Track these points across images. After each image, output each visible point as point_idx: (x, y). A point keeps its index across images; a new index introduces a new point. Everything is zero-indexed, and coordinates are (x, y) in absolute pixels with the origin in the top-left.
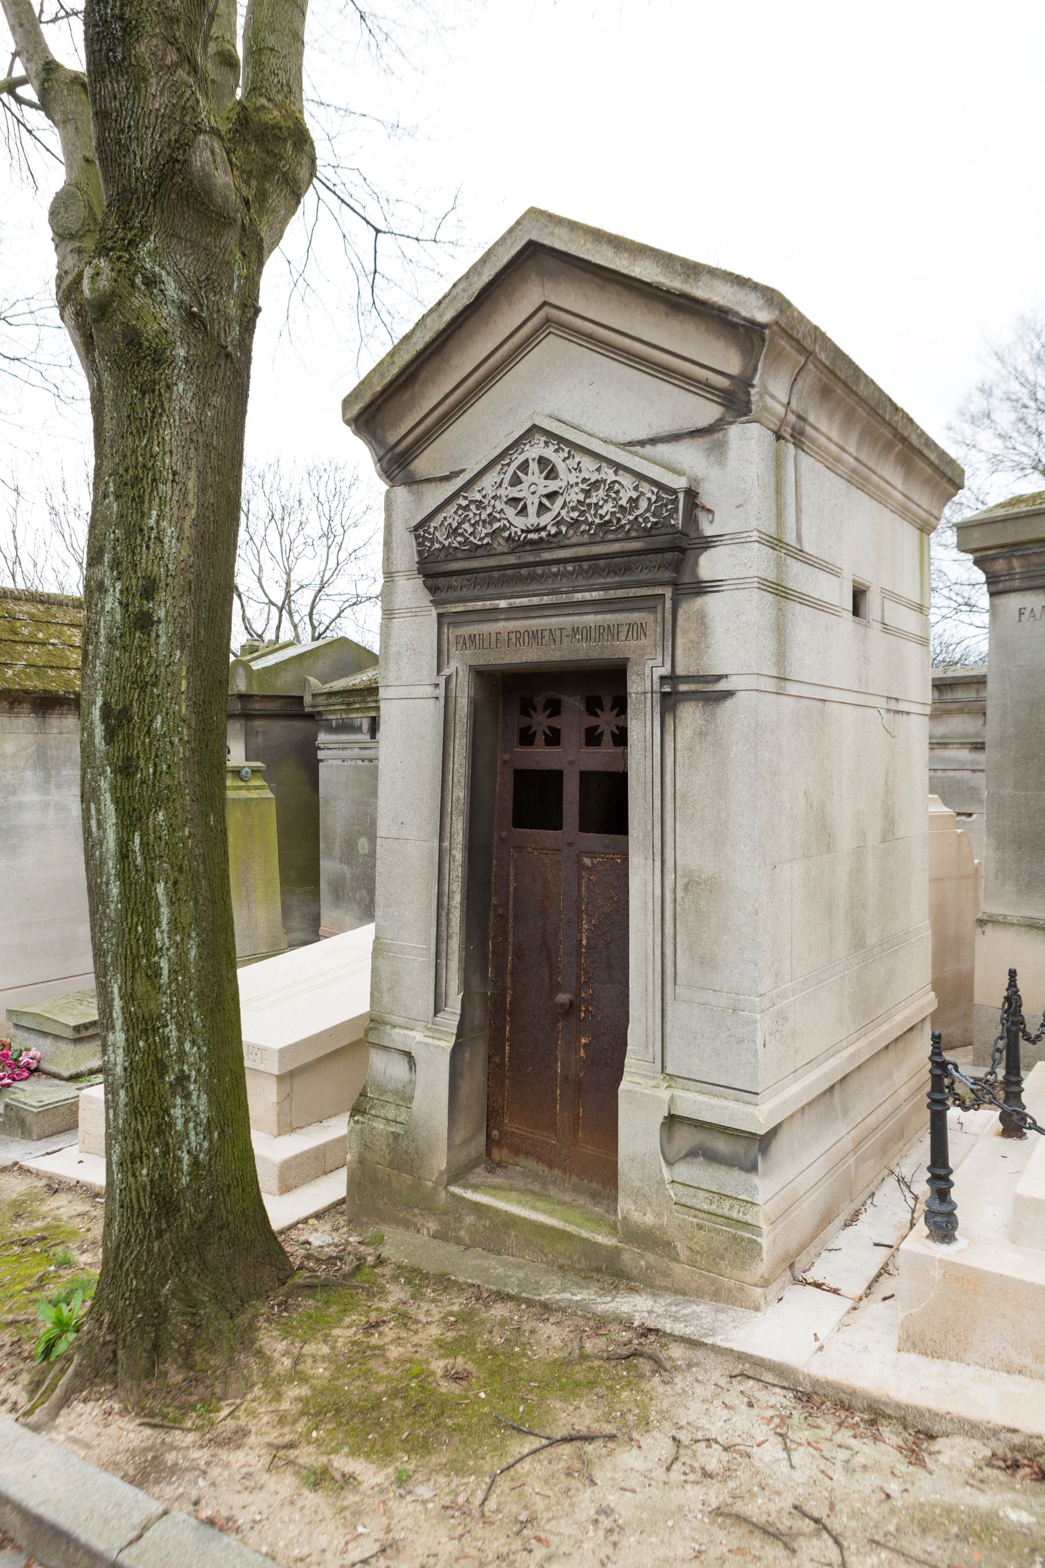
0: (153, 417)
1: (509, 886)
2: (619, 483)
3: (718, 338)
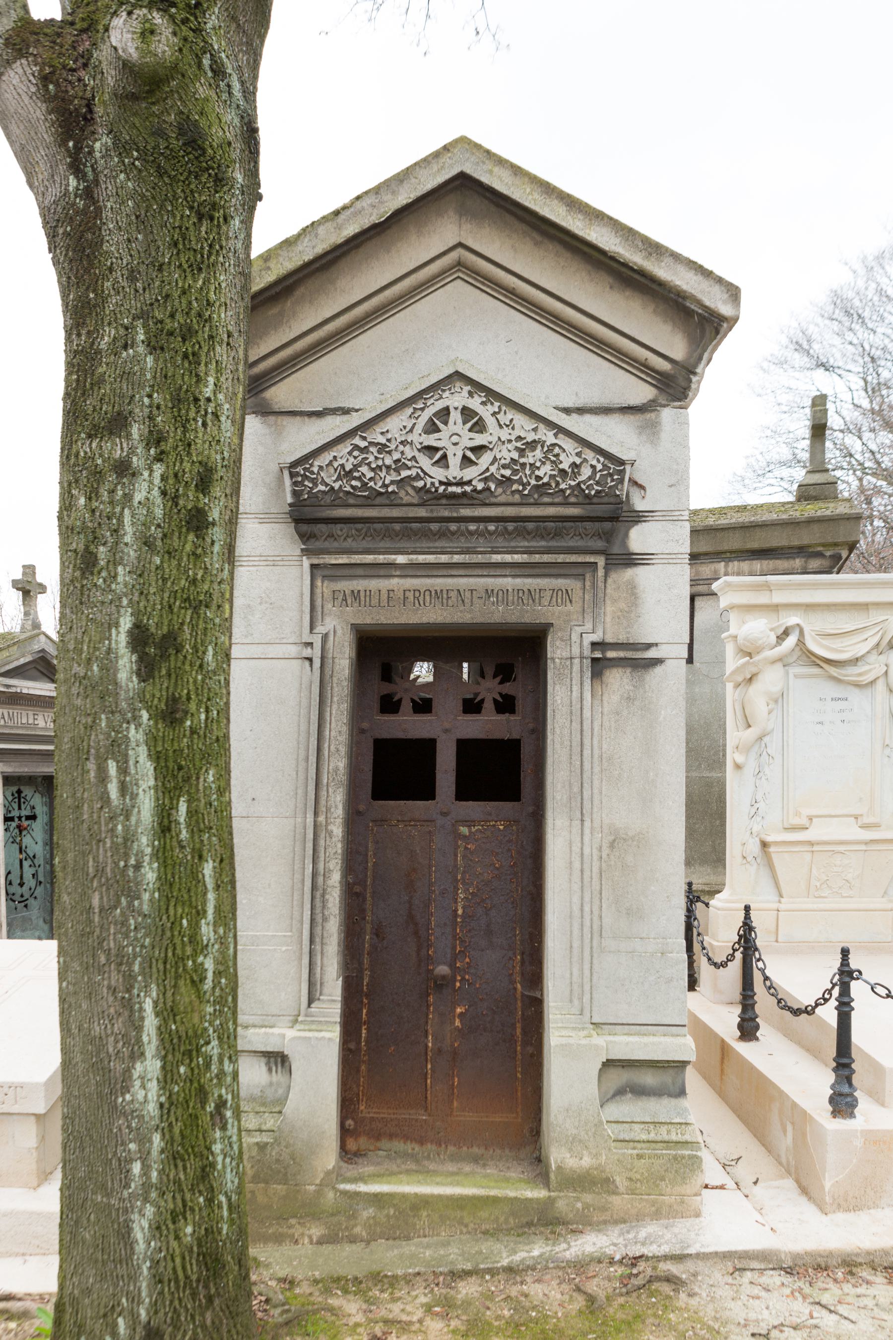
0: (210, 254)
1: (367, 862)
2: (560, 447)
3: (665, 322)
